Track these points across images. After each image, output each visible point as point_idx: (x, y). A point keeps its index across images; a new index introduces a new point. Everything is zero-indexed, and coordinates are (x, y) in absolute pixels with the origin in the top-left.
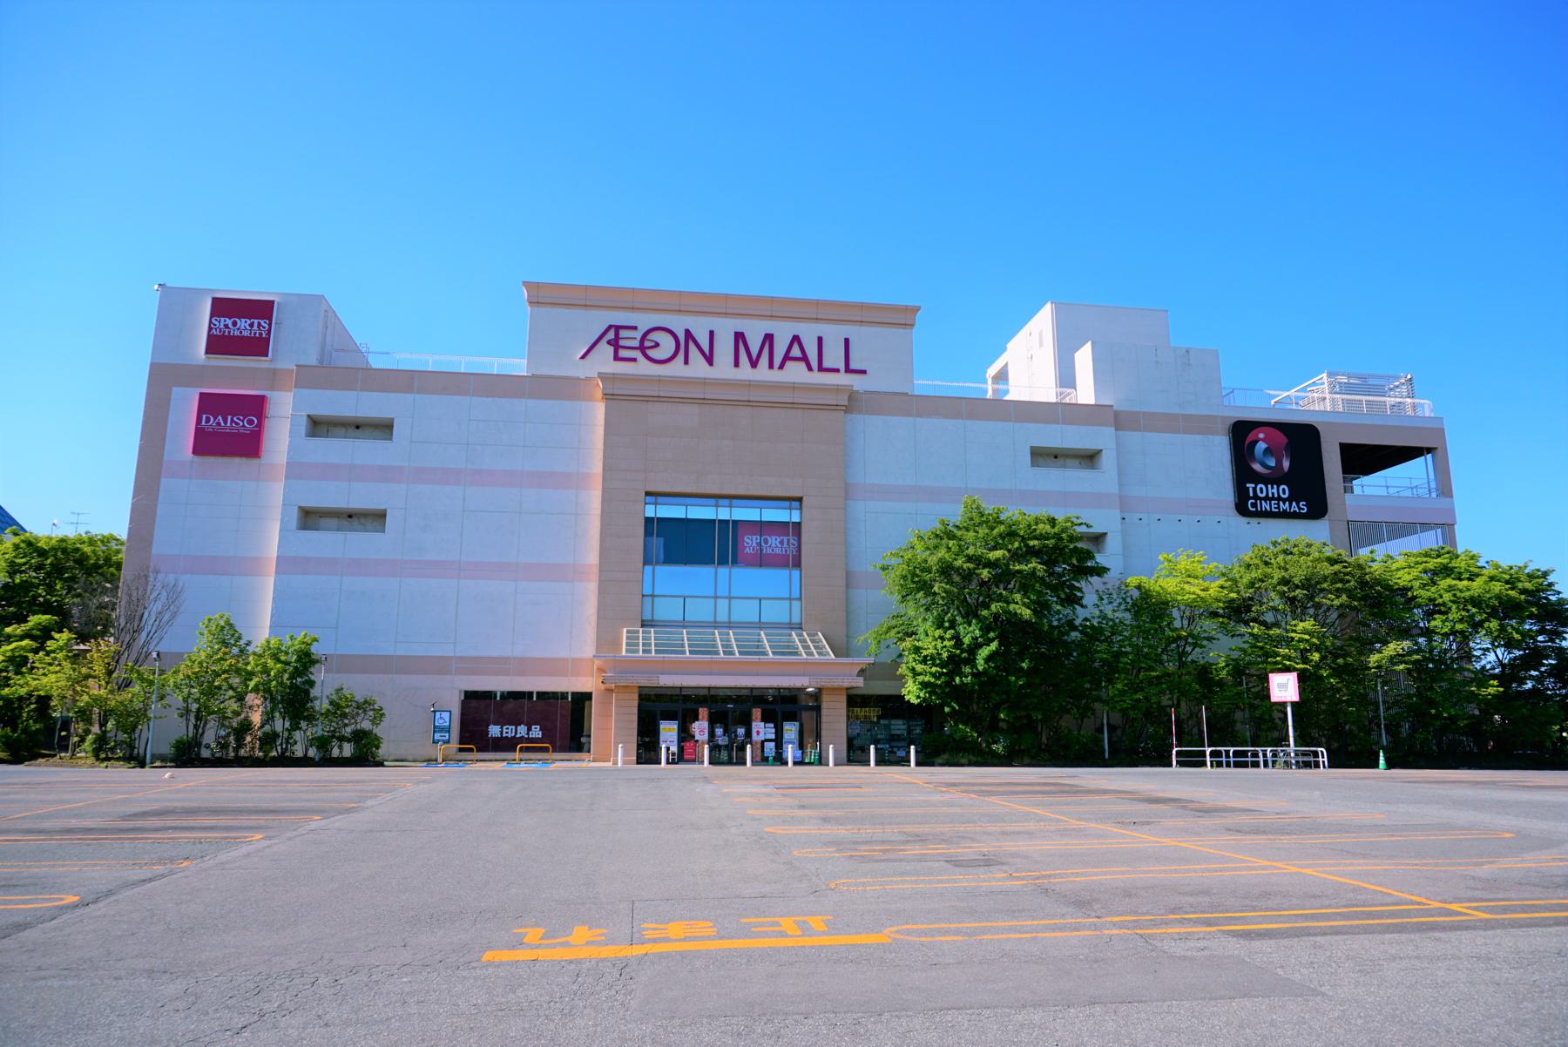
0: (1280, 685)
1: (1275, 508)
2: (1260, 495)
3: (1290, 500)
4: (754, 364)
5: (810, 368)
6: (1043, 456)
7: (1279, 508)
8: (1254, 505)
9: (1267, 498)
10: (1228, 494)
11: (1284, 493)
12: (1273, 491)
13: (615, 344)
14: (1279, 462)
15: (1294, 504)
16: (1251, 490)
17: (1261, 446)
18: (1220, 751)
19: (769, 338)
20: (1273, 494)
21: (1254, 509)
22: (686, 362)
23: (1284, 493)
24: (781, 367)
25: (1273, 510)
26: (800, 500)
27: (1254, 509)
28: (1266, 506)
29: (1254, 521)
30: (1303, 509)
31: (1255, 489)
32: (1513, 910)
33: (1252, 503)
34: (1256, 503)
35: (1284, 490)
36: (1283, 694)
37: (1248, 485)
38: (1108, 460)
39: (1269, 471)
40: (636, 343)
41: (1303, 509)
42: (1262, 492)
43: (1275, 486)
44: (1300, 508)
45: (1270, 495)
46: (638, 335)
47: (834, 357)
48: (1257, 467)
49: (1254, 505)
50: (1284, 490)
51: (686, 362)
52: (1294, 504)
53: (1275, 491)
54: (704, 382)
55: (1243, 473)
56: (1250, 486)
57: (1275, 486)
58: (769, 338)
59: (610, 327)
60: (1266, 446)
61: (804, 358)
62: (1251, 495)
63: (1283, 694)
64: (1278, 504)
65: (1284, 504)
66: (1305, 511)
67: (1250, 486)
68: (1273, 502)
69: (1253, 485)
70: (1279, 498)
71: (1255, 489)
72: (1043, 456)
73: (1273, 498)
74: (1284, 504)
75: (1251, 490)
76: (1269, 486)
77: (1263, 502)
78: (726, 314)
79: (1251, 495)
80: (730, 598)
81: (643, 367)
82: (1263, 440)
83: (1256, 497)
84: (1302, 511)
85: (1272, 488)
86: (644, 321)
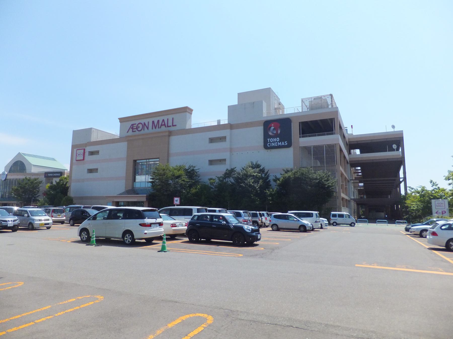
0: (176, 200)
1: (276, 145)
2: (271, 141)
3: (279, 142)
4: (155, 128)
5: (166, 127)
6: (212, 140)
7: (278, 145)
8: (269, 145)
9: (273, 142)
10: (262, 144)
11: (278, 140)
12: (275, 140)
13: (132, 128)
14: (277, 132)
15: (283, 142)
16: (269, 140)
17: (273, 128)
18: (312, 214)
19: (158, 121)
20: (275, 141)
21: (269, 146)
22: (144, 130)
23: (278, 140)
24: (160, 127)
25: (276, 145)
26: (135, 161)
27: (269, 146)
28: (273, 144)
29: (269, 150)
30: (286, 144)
31: (270, 140)
32: (230, 256)
33: (269, 144)
34: (270, 144)
35: (278, 139)
36: (176, 202)
37: (268, 139)
38: (228, 139)
39: (274, 135)
40: (136, 127)
41: (286, 144)
42: (272, 141)
43: (275, 139)
44: (285, 144)
45: (274, 141)
46: (136, 125)
47: (170, 124)
48: (270, 133)
49: (269, 145)
50: (278, 139)
51: (144, 130)
52: (283, 142)
53: (275, 140)
54: (147, 134)
55: (266, 136)
56: (269, 139)
57: (275, 139)
58: (158, 121)
59: (132, 125)
60: (274, 128)
61: (165, 125)
62: (269, 142)
63: (176, 202)
64: (278, 143)
65: (280, 143)
66: (287, 144)
67: (269, 139)
68: (276, 143)
69: (269, 139)
70: (277, 141)
71: (270, 140)
72: (212, 140)
73: (275, 142)
74: (280, 143)
75: (269, 140)
76: (274, 139)
77: (273, 143)
78: (176, 113)
79: (269, 142)
80: (146, 182)
81: (137, 133)
82: (273, 126)
83: (270, 142)
84: (285, 145)
85: (275, 139)
86: (137, 122)
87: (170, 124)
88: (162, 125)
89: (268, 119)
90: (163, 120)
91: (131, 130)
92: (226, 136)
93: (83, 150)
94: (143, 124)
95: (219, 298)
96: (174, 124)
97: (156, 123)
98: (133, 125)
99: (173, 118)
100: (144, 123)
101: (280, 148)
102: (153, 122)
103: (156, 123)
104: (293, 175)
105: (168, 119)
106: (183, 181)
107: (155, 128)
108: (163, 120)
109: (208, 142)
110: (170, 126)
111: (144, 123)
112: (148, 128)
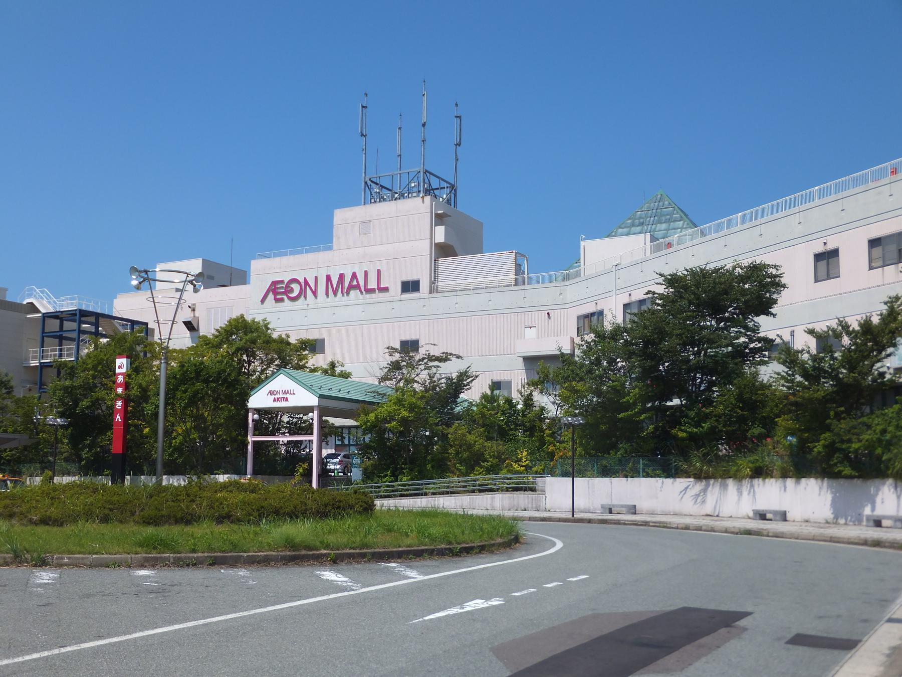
4: (335, 293)
13: (275, 293)
19: (342, 276)
24: (348, 293)
58: (342, 276)
61: (358, 287)
87: (372, 285)
88: (351, 287)
89: (863, 648)
90: (354, 276)
91: (271, 296)
92: (401, 294)
93: (45, 331)
94: (302, 281)
95: (98, 536)
96: (382, 286)
97: (335, 281)
98: (274, 283)
99: (379, 271)
100: (305, 280)
101: (193, 258)
102: (328, 278)
103: (335, 281)
104: (59, 447)
105: (366, 272)
106: (421, 365)
107: (335, 293)
108: (354, 276)
109: (283, 303)
110: (372, 291)
111: (305, 280)
112: (315, 293)
